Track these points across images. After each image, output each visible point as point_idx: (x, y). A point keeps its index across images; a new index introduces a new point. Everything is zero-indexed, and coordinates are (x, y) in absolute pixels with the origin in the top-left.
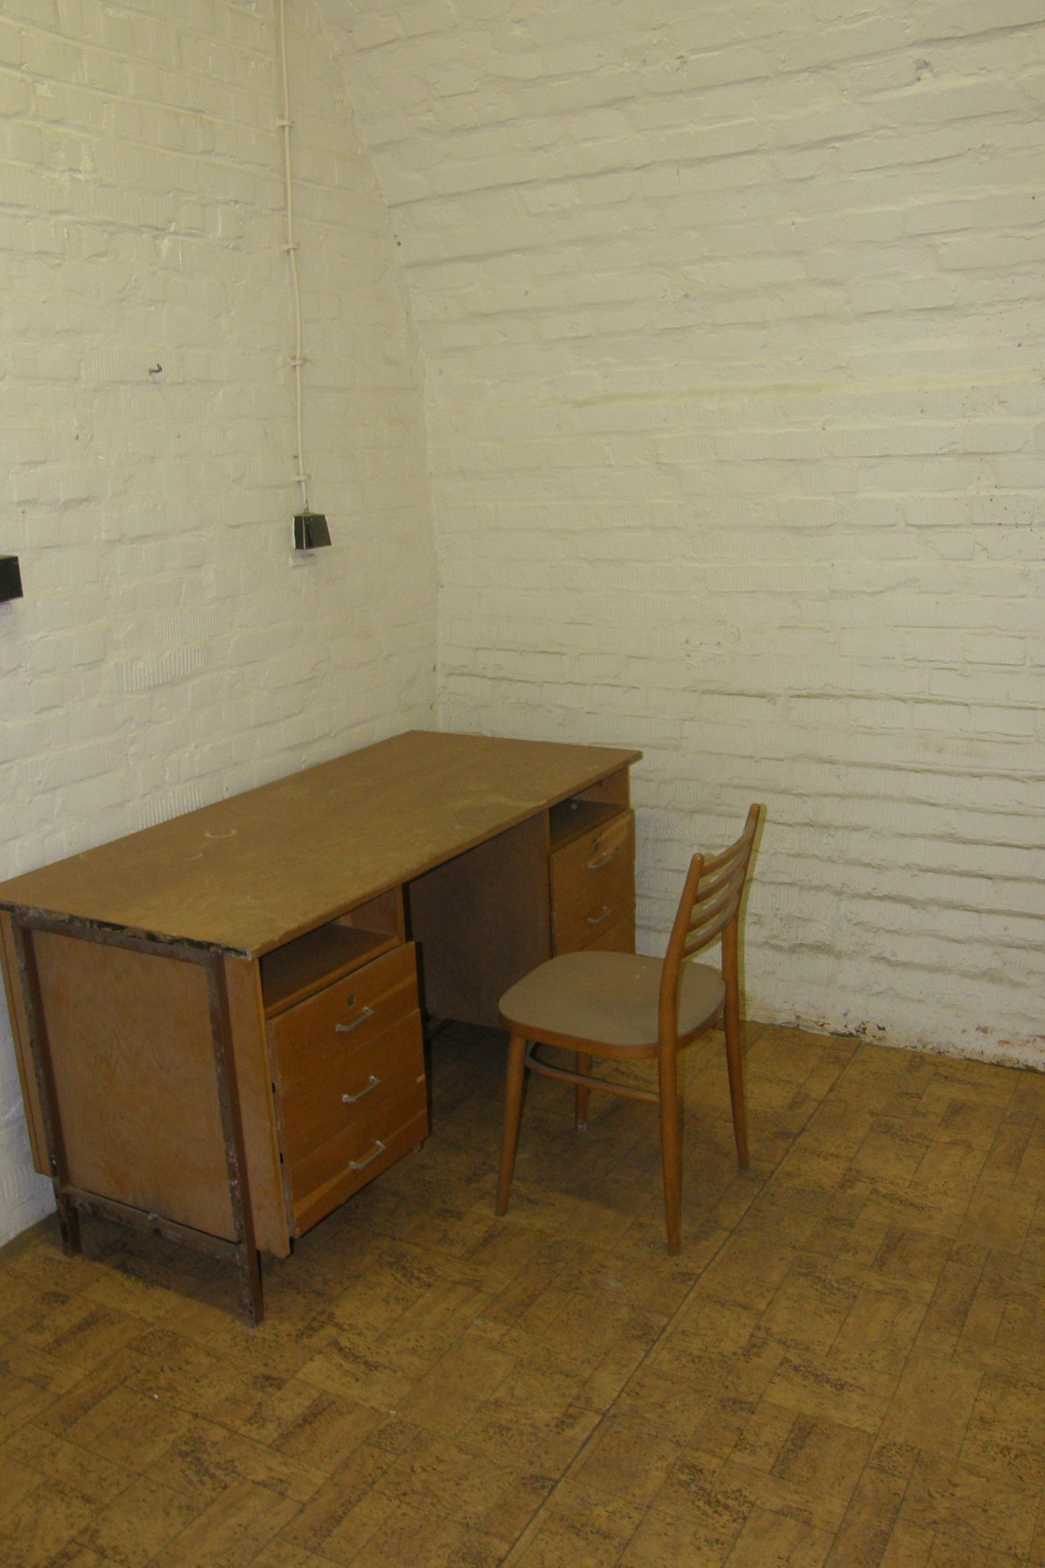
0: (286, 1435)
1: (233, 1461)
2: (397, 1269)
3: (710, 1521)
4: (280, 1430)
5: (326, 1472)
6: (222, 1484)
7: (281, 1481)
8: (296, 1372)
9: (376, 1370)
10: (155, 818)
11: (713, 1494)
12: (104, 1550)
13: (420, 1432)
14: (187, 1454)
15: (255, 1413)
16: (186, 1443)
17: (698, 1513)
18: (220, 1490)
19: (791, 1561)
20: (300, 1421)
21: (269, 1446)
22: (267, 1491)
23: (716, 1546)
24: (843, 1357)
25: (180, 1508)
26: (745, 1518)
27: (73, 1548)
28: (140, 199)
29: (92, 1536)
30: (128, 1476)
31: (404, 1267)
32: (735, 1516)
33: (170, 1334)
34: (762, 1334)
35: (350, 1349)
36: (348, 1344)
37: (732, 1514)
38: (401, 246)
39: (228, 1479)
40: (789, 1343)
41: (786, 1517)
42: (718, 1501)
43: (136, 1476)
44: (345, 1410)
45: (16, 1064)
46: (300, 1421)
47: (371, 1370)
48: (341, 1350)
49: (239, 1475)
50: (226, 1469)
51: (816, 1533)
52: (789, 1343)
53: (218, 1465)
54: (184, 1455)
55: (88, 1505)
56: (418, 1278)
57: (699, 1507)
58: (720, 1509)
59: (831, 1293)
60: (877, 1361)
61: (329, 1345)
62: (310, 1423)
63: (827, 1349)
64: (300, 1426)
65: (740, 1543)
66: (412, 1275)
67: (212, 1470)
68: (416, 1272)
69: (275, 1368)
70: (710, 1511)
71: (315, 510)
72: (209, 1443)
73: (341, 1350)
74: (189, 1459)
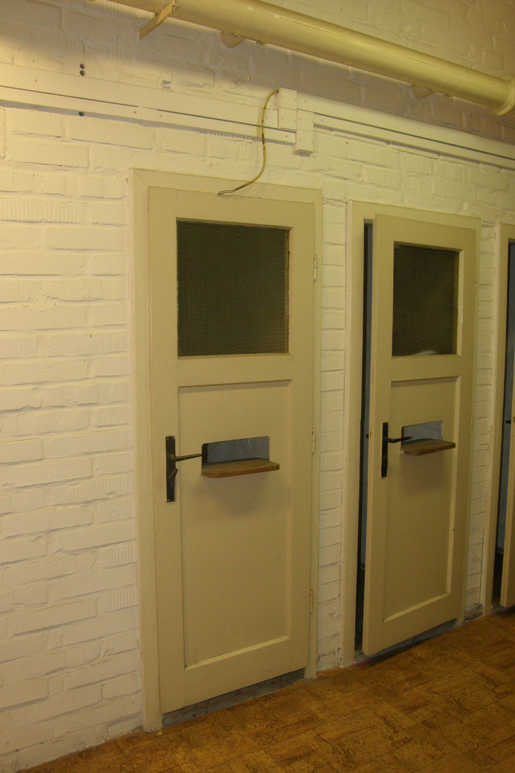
0: (308, 755)
1: (333, 753)
2: (463, 706)
4: (310, 758)
5: (298, 737)
6: (340, 746)
7: (317, 740)
8: (416, 725)
9: (382, 716)
10: (503, 88)
12: (390, 739)
13: (255, 738)
14: (352, 762)
15: (317, 768)
16: (351, 767)
18: (342, 744)
20: (419, 708)
21: (316, 753)
22: (324, 738)
25: (359, 743)
26: (339, 744)
27: (402, 743)
29: (394, 745)
30: (378, 761)
31: (347, 758)
33: (476, 762)
35: (390, 728)
36: (390, 730)
39: (337, 747)
42: (345, 753)
43: (374, 760)
44: (278, 757)
46: (419, 708)
47: (384, 717)
48: (394, 728)
49: (333, 747)
50: (337, 751)
53: (452, 703)
54: (353, 762)
55: (396, 756)
56: (455, 700)
61: (398, 732)
62: (415, 706)
64: (300, 757)
66: (457, 702)
67: (343, 752)
68: (455, 703)
69: (425, 729)
72: (341, 763)
73: (394, 728)
74: (351, 760)
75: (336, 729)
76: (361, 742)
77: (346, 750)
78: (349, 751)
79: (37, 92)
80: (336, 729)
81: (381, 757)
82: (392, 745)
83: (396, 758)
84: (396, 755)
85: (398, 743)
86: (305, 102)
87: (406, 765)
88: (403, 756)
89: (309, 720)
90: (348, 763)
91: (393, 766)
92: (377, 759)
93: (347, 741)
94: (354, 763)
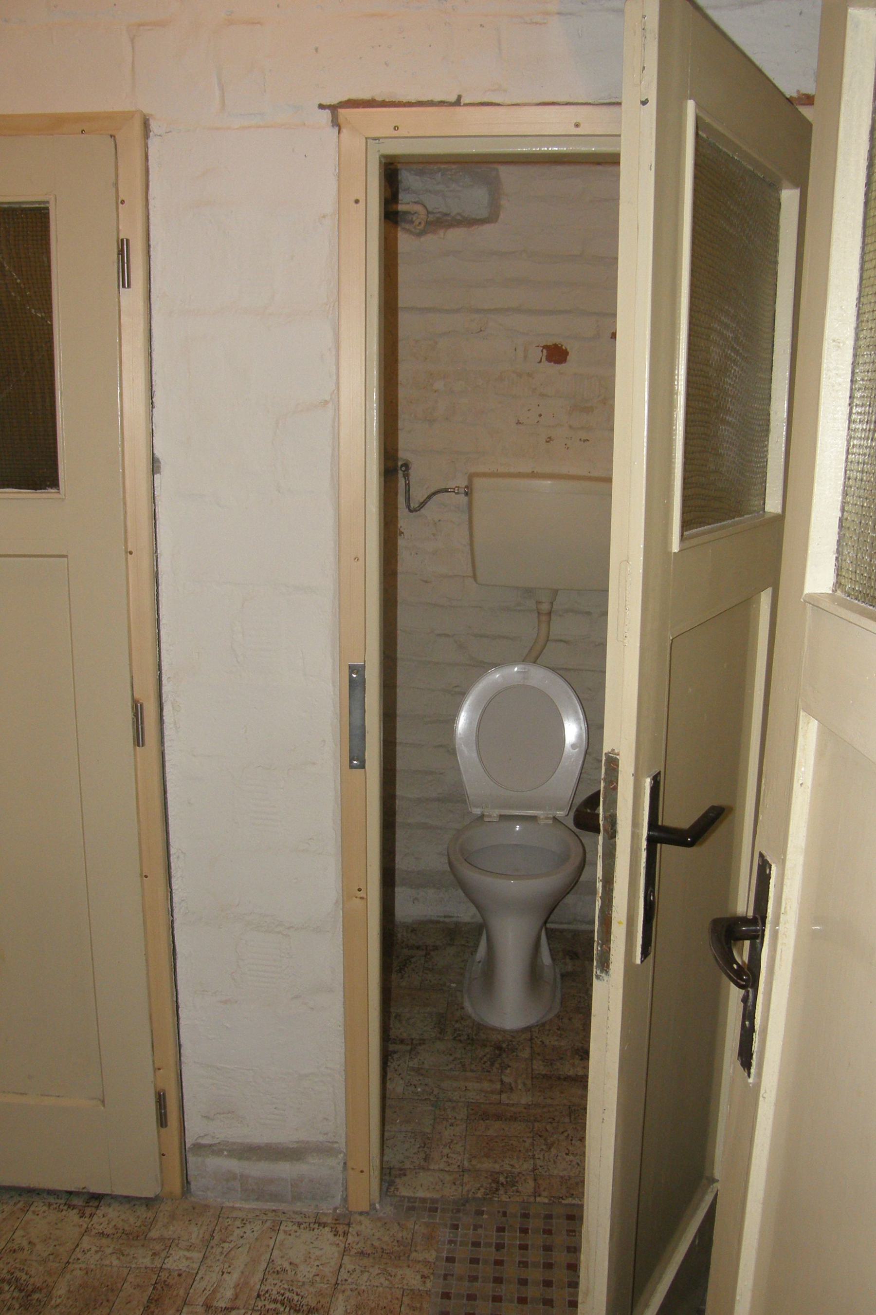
3: (286, 1286)
11: (287, 1309)
17: (297, 1290)
19: (221, 1273)
23: (278, 1268)
24: (268, 1224)
26: (259, 1296)
28: (698, 69)
32: (267, 1295)
34: (341, 1229)
37: (269, 1296)
38: (355, 198)
40: (316, 1226)
41: (225, 1308)
42: (283, 1304)
45: (868, 149)
51: (201, 1301)
52: (316, 1226)
57: (297, 1294)
58: (280, 1298)
59: (283, 1295)
60: (238, 1228)
63: (282, 1228)
65: (260, 1275)
70: (288, 1294)
71: (317, 106)
74: (494, 1185)
75: (223, 1273)
76: (25, 1243)
77: (280, 1298)
78: (286, 1295)
79: (553, 104)
80: (223, 1273)
81: (78, 1249)
82: (81, 1217)
83: (102, 1234)
84: (100, 1228)
85: (88, 1206)
86: (124, 201)
87: (127, 1234)
88: (113, 1223)
89: (160, 1288)
90: (29, 1298)
91: (109, 1251)
92: (73, 1257)
93: (263, 1280)
94: (40, 1290)
